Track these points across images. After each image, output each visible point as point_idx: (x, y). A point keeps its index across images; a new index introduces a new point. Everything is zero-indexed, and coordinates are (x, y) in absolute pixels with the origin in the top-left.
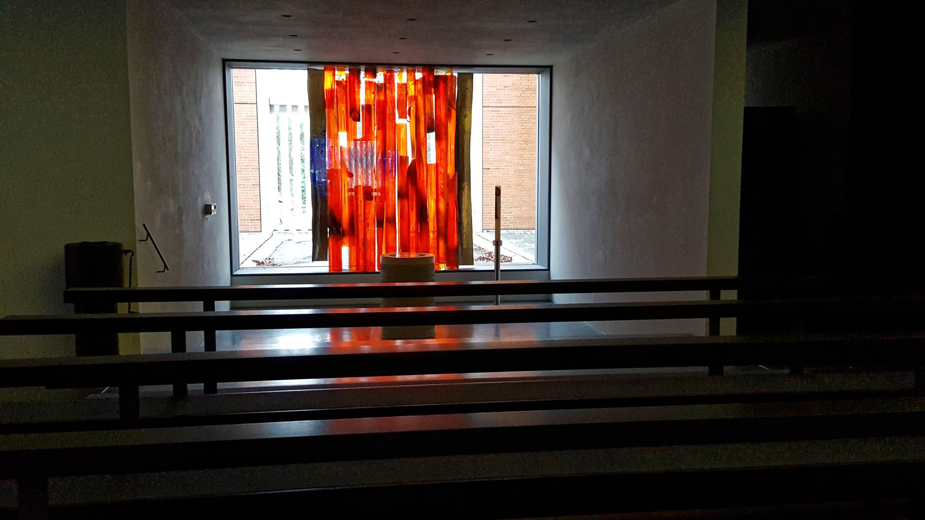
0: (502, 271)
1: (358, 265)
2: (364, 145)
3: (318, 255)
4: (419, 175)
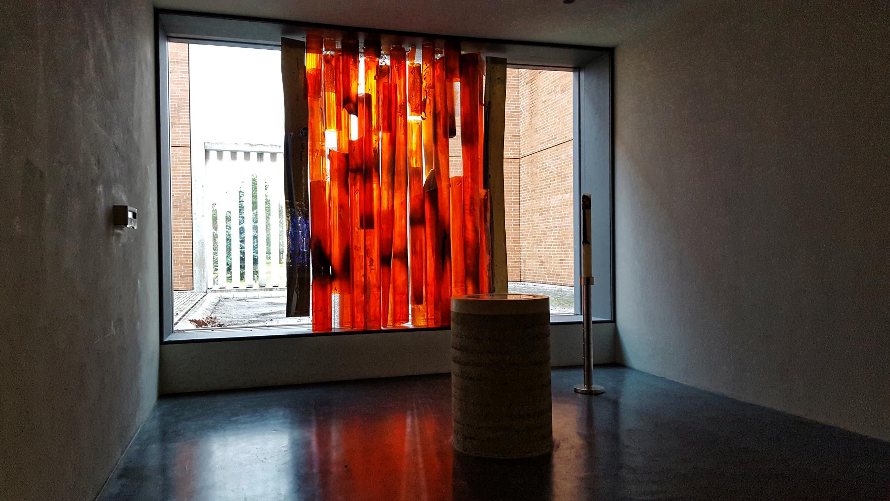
0: (594, 322)
1: (353, 322)
3: (296, 308)
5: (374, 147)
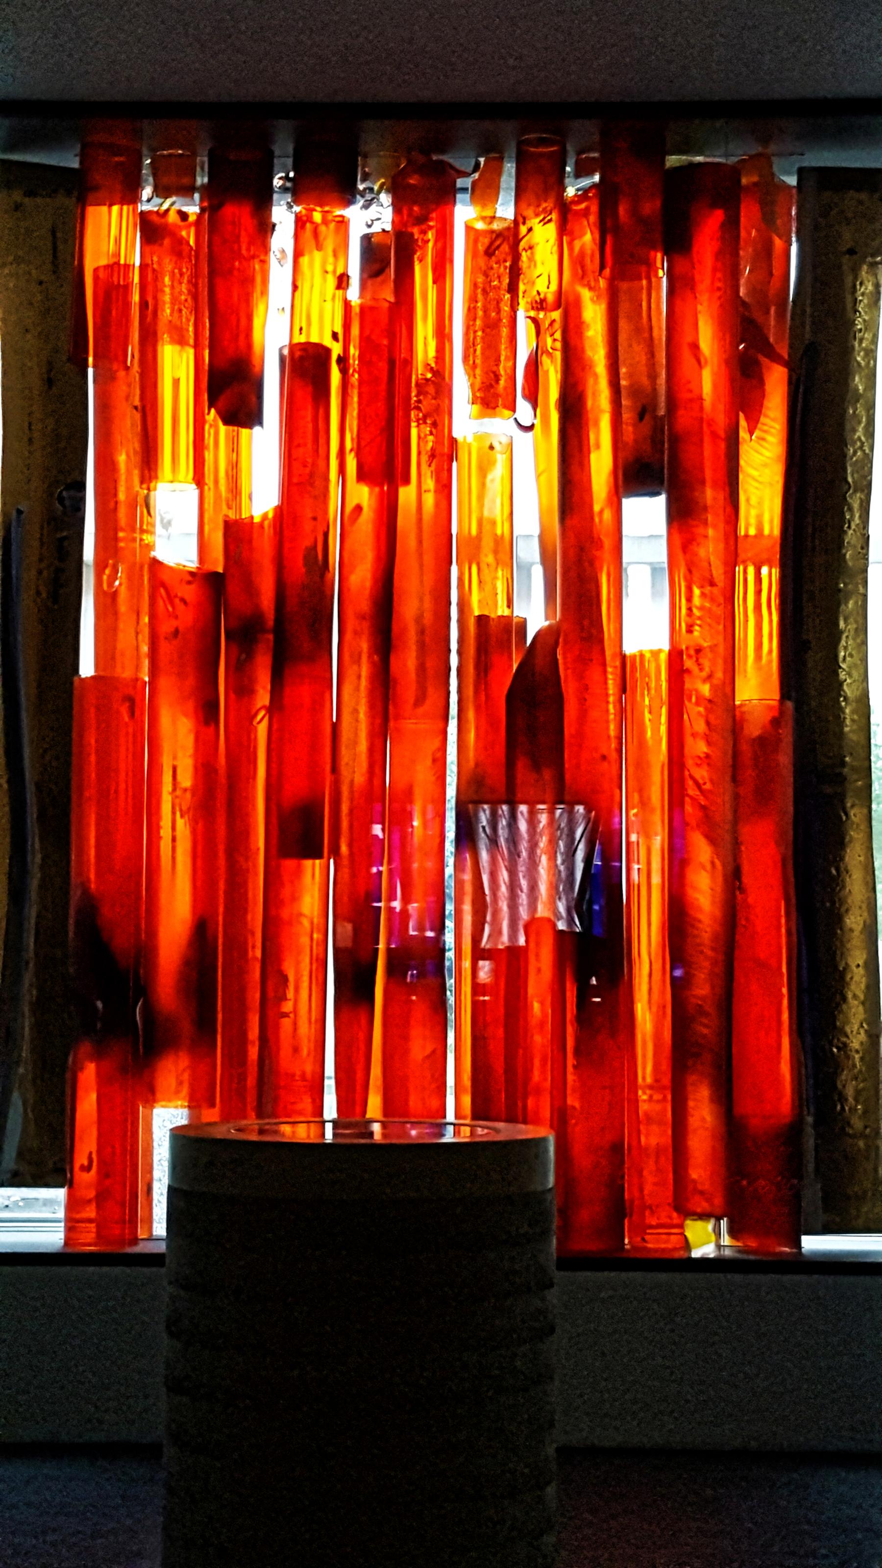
2: (543, 819)
4: (583, 714)
5: (307, 543)
